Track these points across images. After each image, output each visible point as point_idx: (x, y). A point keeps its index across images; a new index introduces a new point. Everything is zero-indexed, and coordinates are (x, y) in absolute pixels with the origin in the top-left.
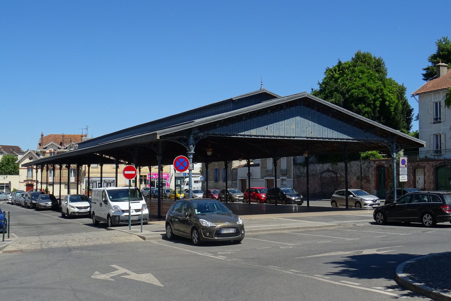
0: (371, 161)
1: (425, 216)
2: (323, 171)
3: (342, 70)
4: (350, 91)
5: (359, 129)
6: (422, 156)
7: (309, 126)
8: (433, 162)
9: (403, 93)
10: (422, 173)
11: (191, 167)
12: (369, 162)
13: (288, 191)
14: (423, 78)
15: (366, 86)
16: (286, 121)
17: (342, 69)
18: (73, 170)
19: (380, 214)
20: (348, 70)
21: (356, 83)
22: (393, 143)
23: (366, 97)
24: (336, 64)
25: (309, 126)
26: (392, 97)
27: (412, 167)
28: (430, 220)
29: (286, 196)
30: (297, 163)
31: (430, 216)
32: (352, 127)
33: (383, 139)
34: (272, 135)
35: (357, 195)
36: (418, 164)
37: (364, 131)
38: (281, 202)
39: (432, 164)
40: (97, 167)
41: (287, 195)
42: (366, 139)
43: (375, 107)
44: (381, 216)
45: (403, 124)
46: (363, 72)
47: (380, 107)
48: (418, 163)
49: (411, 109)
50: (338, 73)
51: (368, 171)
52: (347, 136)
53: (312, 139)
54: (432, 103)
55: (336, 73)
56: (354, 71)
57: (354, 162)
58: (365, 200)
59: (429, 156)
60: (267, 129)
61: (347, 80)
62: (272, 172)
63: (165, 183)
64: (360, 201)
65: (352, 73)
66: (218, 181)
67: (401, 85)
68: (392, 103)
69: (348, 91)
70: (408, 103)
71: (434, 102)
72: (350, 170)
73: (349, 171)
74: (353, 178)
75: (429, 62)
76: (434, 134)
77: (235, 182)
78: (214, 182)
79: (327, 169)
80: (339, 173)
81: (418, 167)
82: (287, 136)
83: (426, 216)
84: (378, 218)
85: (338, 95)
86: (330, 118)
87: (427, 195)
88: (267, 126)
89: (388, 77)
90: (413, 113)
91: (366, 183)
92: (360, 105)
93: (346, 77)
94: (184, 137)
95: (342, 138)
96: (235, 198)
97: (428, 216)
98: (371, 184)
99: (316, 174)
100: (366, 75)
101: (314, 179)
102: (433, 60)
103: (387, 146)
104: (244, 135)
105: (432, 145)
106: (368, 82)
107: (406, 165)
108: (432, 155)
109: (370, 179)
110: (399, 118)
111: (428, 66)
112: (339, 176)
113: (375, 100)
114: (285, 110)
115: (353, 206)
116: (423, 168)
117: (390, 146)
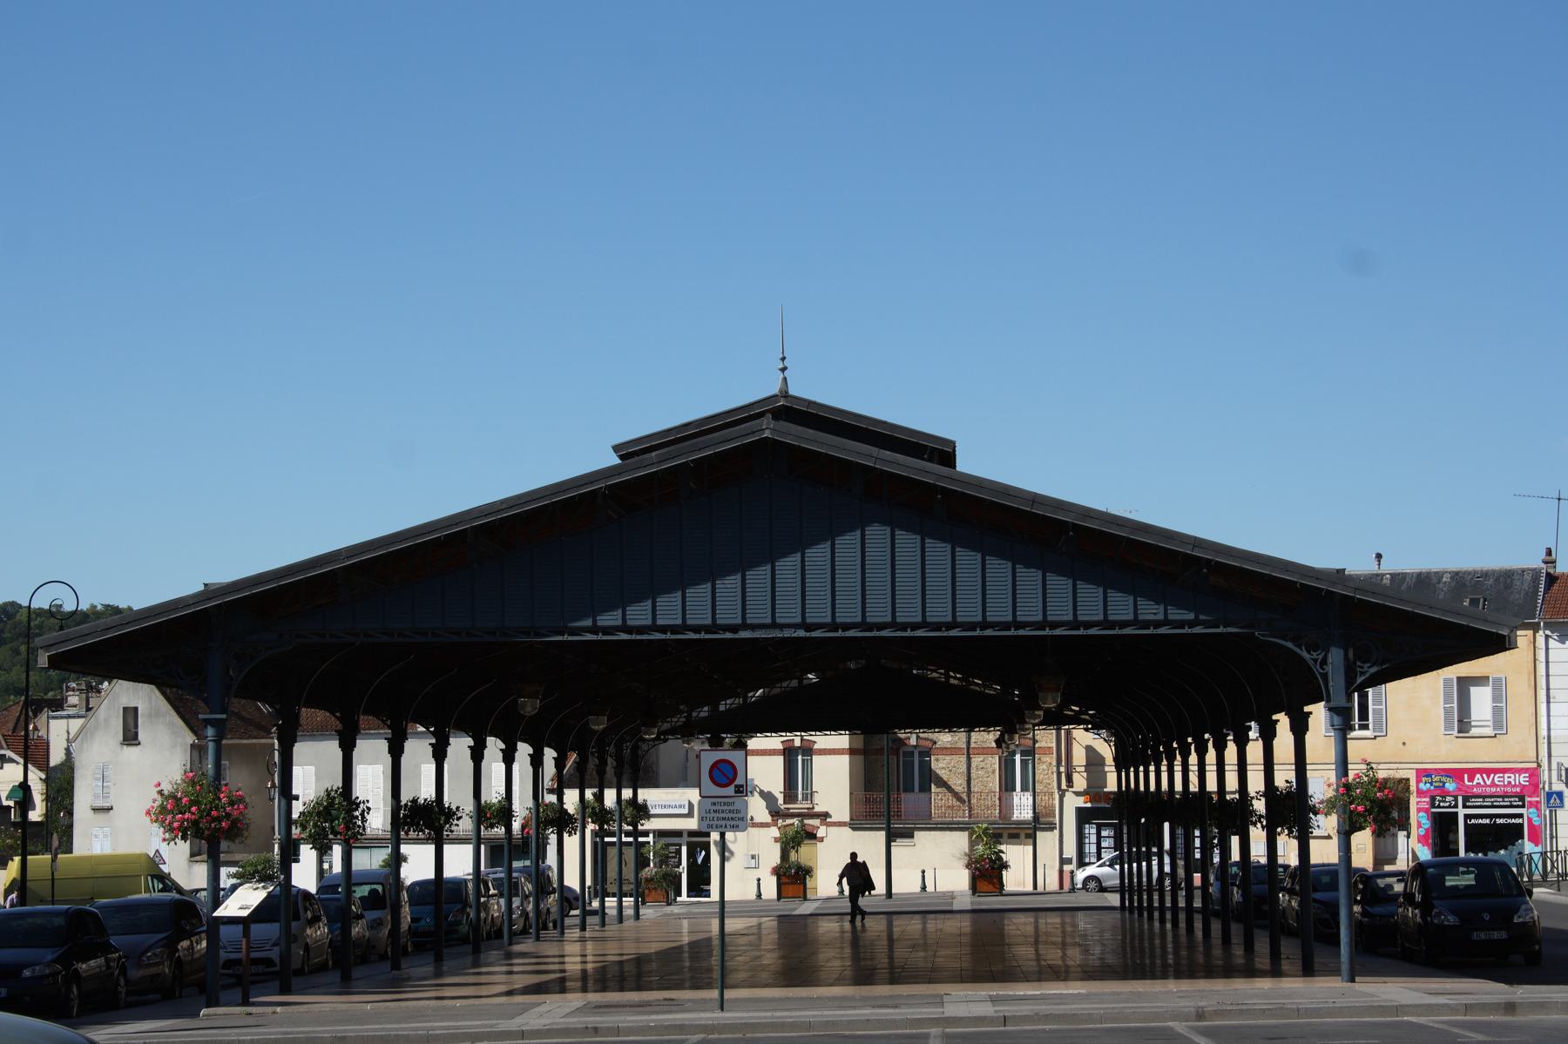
53: (871, 630)
63: (1520, 821)
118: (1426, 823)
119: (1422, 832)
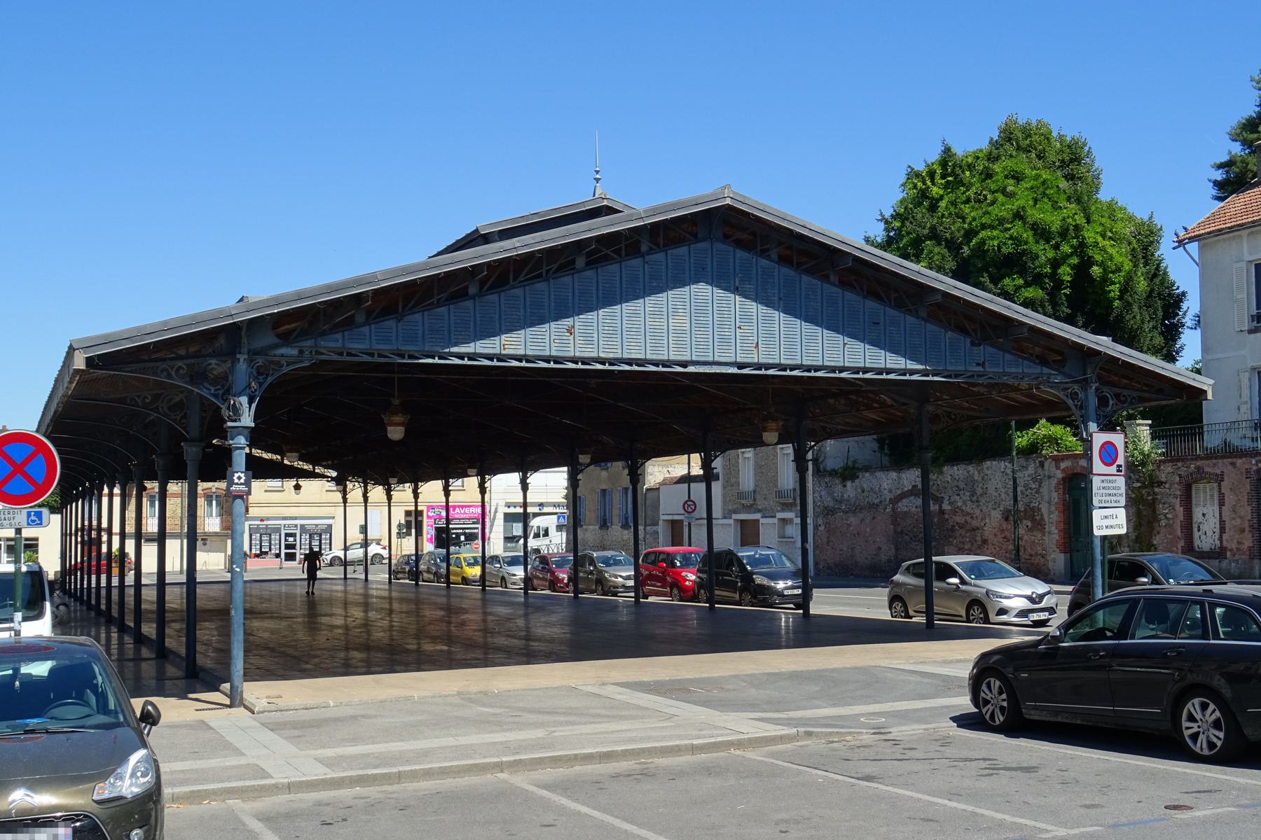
0: (1046, 459)
1: (1189, 705)
2: (899, 492)
3: (952, 172)
4: (976, 233)
5: (950, 334)
6: (1212, 440)
7: (746, 318)
8: (1249, 459)
9: (1152, 242)
10: (1212, 496)
11: (237, 484)
12: (1040, 462)
13: (765, 561)
14: (1214, 192)
15: (1029, 219)
16: (650, 300)
17: (954, 168)
18: (214, 497)
19: (996, 684)
20: (971, 171)
21: (996, 211)
22: (1085, 383)
23: (1024, 252)
24: (934, 156)
25: (746, 318)
26: (1110, 250)
27: (1180, 476)
28: (1217, 725)
29: (754, 576)
30: (825, 471)
31: (1212, 707)
32: (923, 322)
33: (1046, 370)
34: (594, 355)
35: (973, 577)
36: (1198, 468)
37: (968, 340)
38: (737, 596)
39: (1247, 466)
40: (461, 488)
41: (757, 573)
42: (980, 369)
43: (1058, 284)
44: (1000, 693)
45: (1151, 340)
46: (1017, 177)
47: (1073, 284)
48: (1199, 463)
49: (1178, 295)
50: (942, 184)
51: (1038, 492)
52: (904, 359)
54: (1243, 265)
55: (933, 184)
56: (987, 175)
57: (994, 463)
58: (1001, 597)
59: (1235, 439)
60: (569, 331)
61: (968, 201)
62: (795, 499)
64: (984, 600)
65: (983, 181)
66: (609, 525)
67: (1146, 218)
68: (1113, 272)
69: (970, 234)
70: (1165, 273)
71: (1251, 262)
72: (981, 491)
73: (979, 493)
74: (989, 515)
75: (1233, 140)
76: (1253, 369)
77: (655, 528)
78: (597, 527)
79: (913, 486)
80: (947, 498)
81: (1200, 476)
82: (654, 357)
83: (1194, 705)
84: (986, 702)
85: (937, 250)
86: (834, 289)
87: (1202, 604)
88: (571, 319)
89: (1104, 195)
90: (1184, 306)
91: (1030, 530)
92: (1007, 281)
93: (963, 194)
94: (210, 364)
95: (883, 366)
96: (613, 581)
97: (1204, 707)
98: (1047, 535)
99: (881, 502)
100: (1028, 186)
101: (874, 518)
102: (1245, 135)
103: (1061, 395)
104: (471, 357)
105: (1246, 403)
106: (1035, 205)
107: (1119, 466)
108: (1245, 437)
109: (1042, 519)
110: (1138, 318)
111: (1230, 152)
112: (949, 508)
113: (1056, 264)
114: (647, 258)
115: (961, 616)
116: (1216, 481)
117: (1074, 396)
118: (433, 532)
119: (429, 536)
